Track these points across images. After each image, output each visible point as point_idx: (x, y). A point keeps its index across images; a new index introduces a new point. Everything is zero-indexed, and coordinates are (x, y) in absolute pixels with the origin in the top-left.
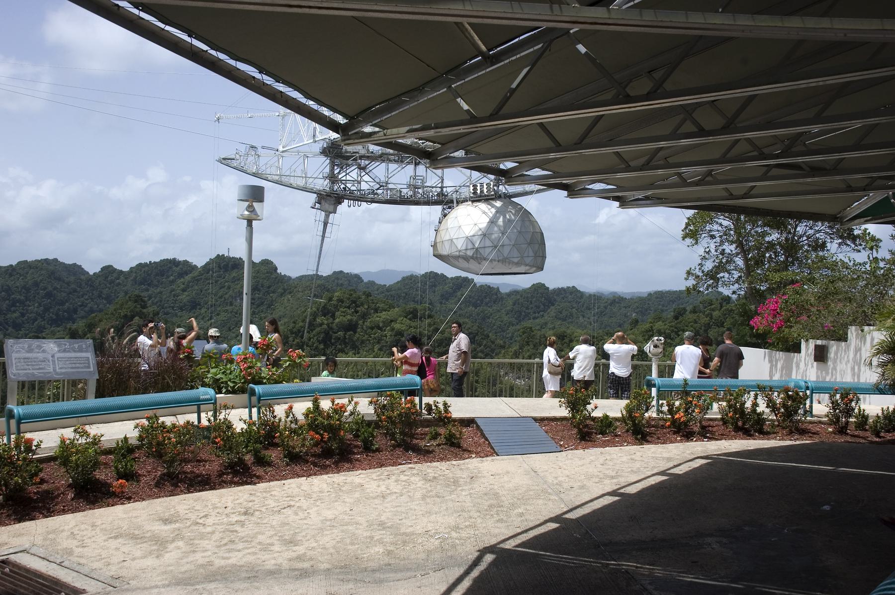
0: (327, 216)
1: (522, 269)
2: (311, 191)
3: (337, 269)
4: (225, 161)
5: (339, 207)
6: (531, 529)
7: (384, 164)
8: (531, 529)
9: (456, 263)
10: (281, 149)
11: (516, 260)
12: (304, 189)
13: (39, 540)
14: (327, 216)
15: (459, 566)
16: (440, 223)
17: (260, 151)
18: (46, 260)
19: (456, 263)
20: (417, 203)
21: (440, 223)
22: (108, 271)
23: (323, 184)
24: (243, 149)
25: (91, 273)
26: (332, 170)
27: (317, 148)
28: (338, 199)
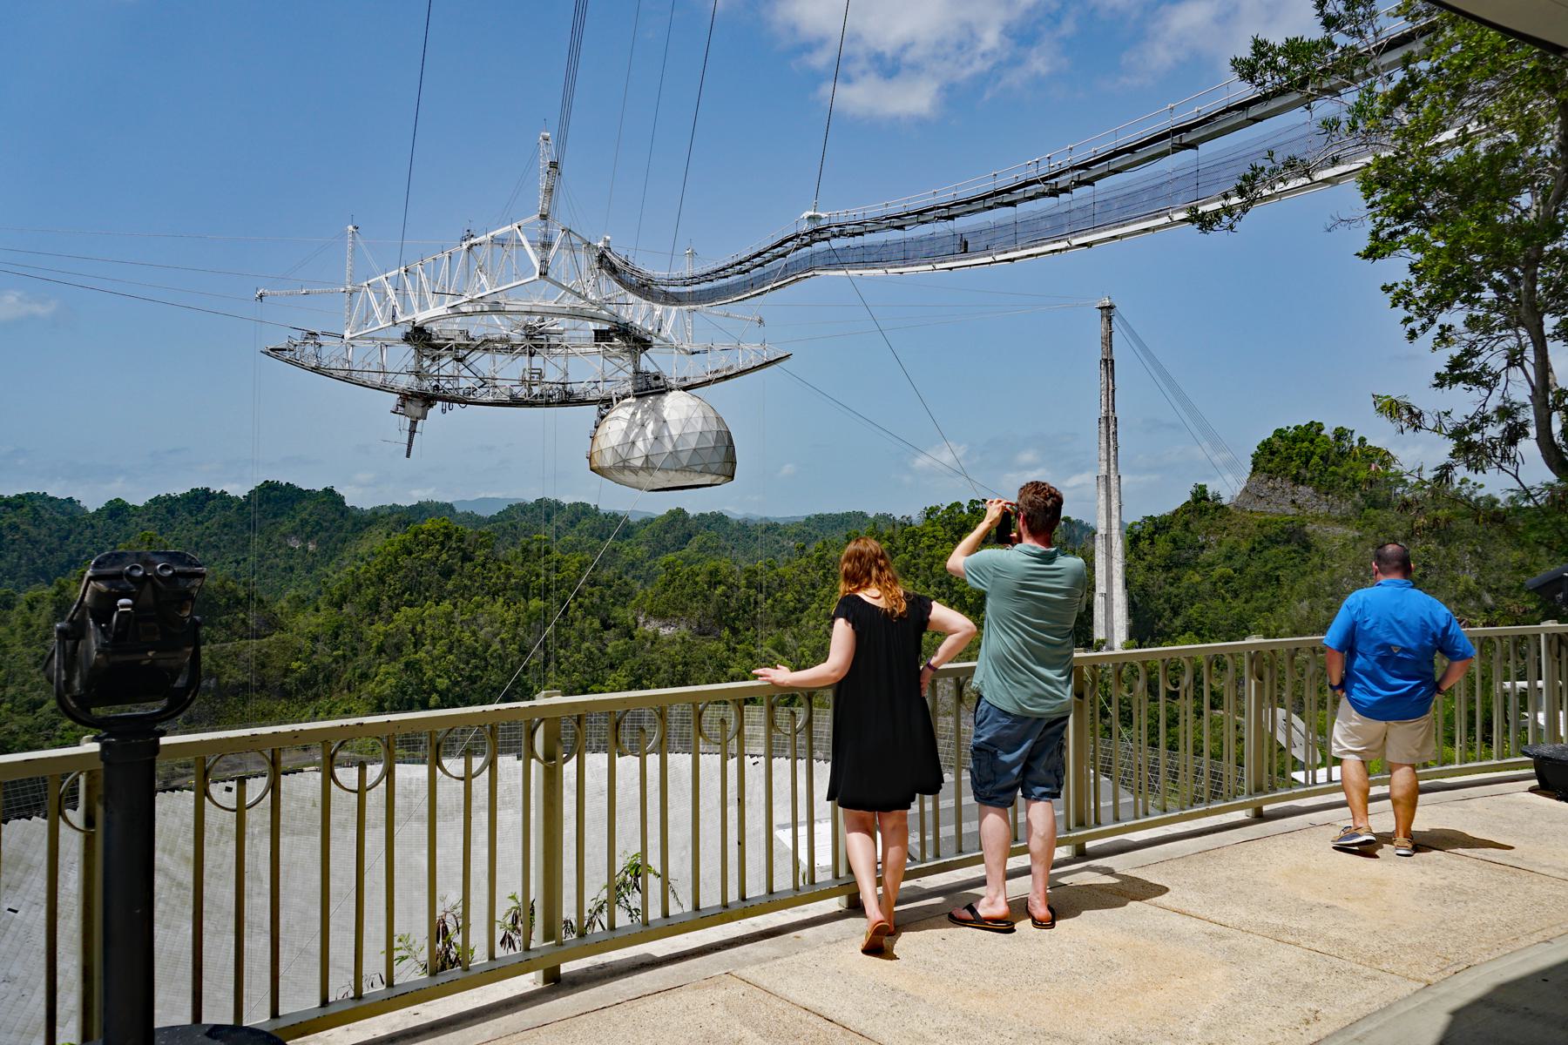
0: (414, 423)
1: (707, 479)
2: (392, 391)
3: (200, 485)
4: (276, 352)
5: (430, 411)
7: (488, 355)
10: (347, 335)
13: (1088, 478)
14: (414, 423)
15: (34, 1035)
20: (533, 405)
23: (406, 382)
24: (298, 337)
27: (399, 333)
28: (428, 400)
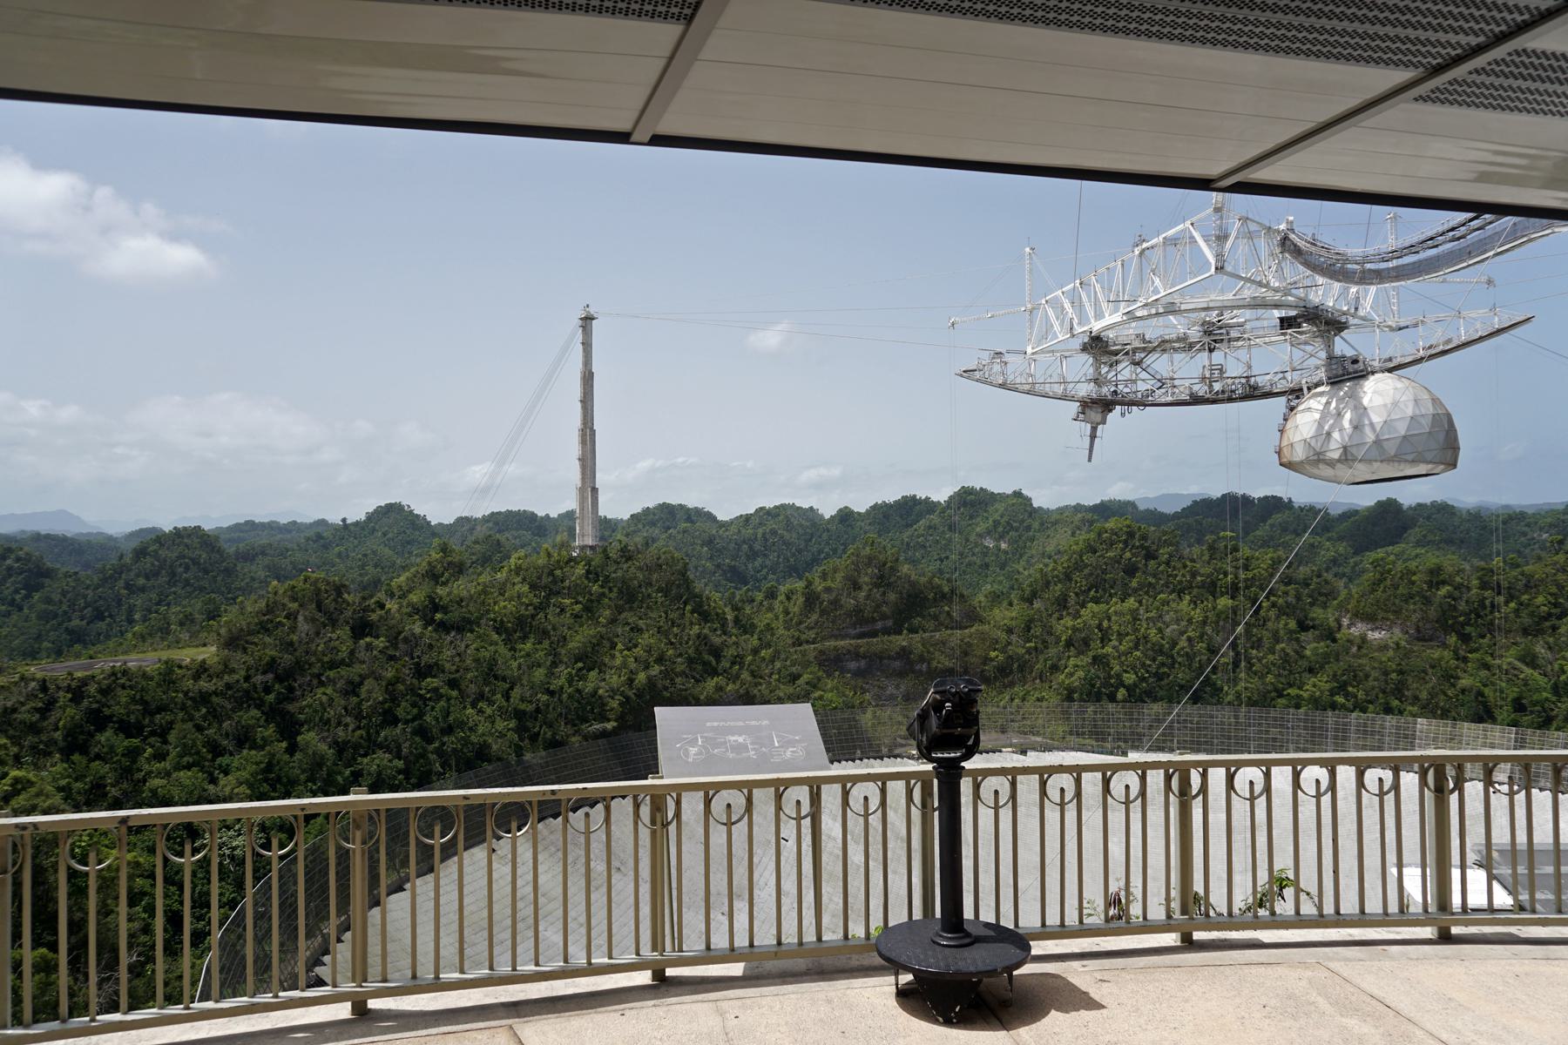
0: (1094, 429)
1: (1422, 469)
5: (1110, 416)
6: (1336, 872)
8: (1336, 872)
9: (1315, 471)
11: (1410, 457)
12: (1064, 398)
14: (1094, 429)
16: (1286, 420)
17: (1007, 358)
18: (237, 525)
19: (1315, 471)
21: (1286, 420)
22: (845, 516)
23: (1086, 390)
24: (986, 357)
25: (827, 517)
26: (1097, 369)
27: (1077, 344)
28: (1106, 405)
